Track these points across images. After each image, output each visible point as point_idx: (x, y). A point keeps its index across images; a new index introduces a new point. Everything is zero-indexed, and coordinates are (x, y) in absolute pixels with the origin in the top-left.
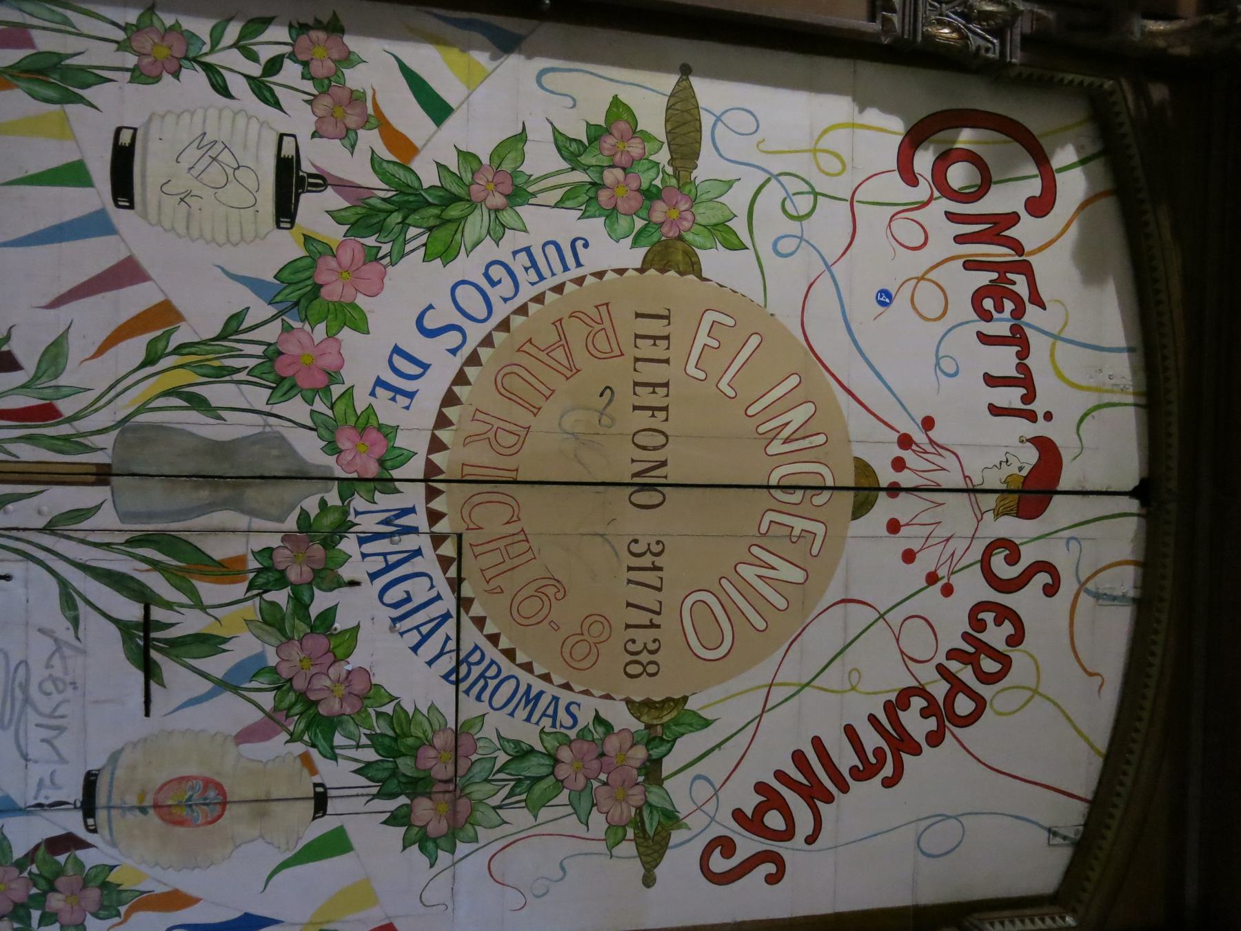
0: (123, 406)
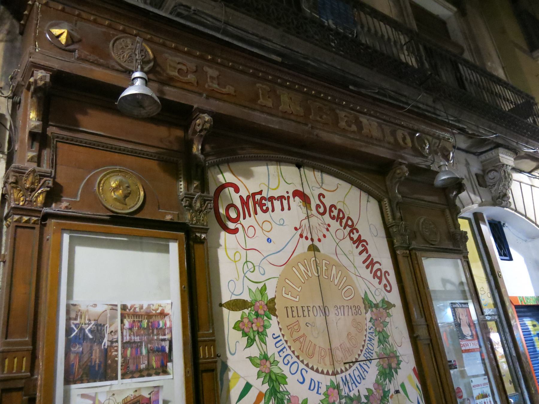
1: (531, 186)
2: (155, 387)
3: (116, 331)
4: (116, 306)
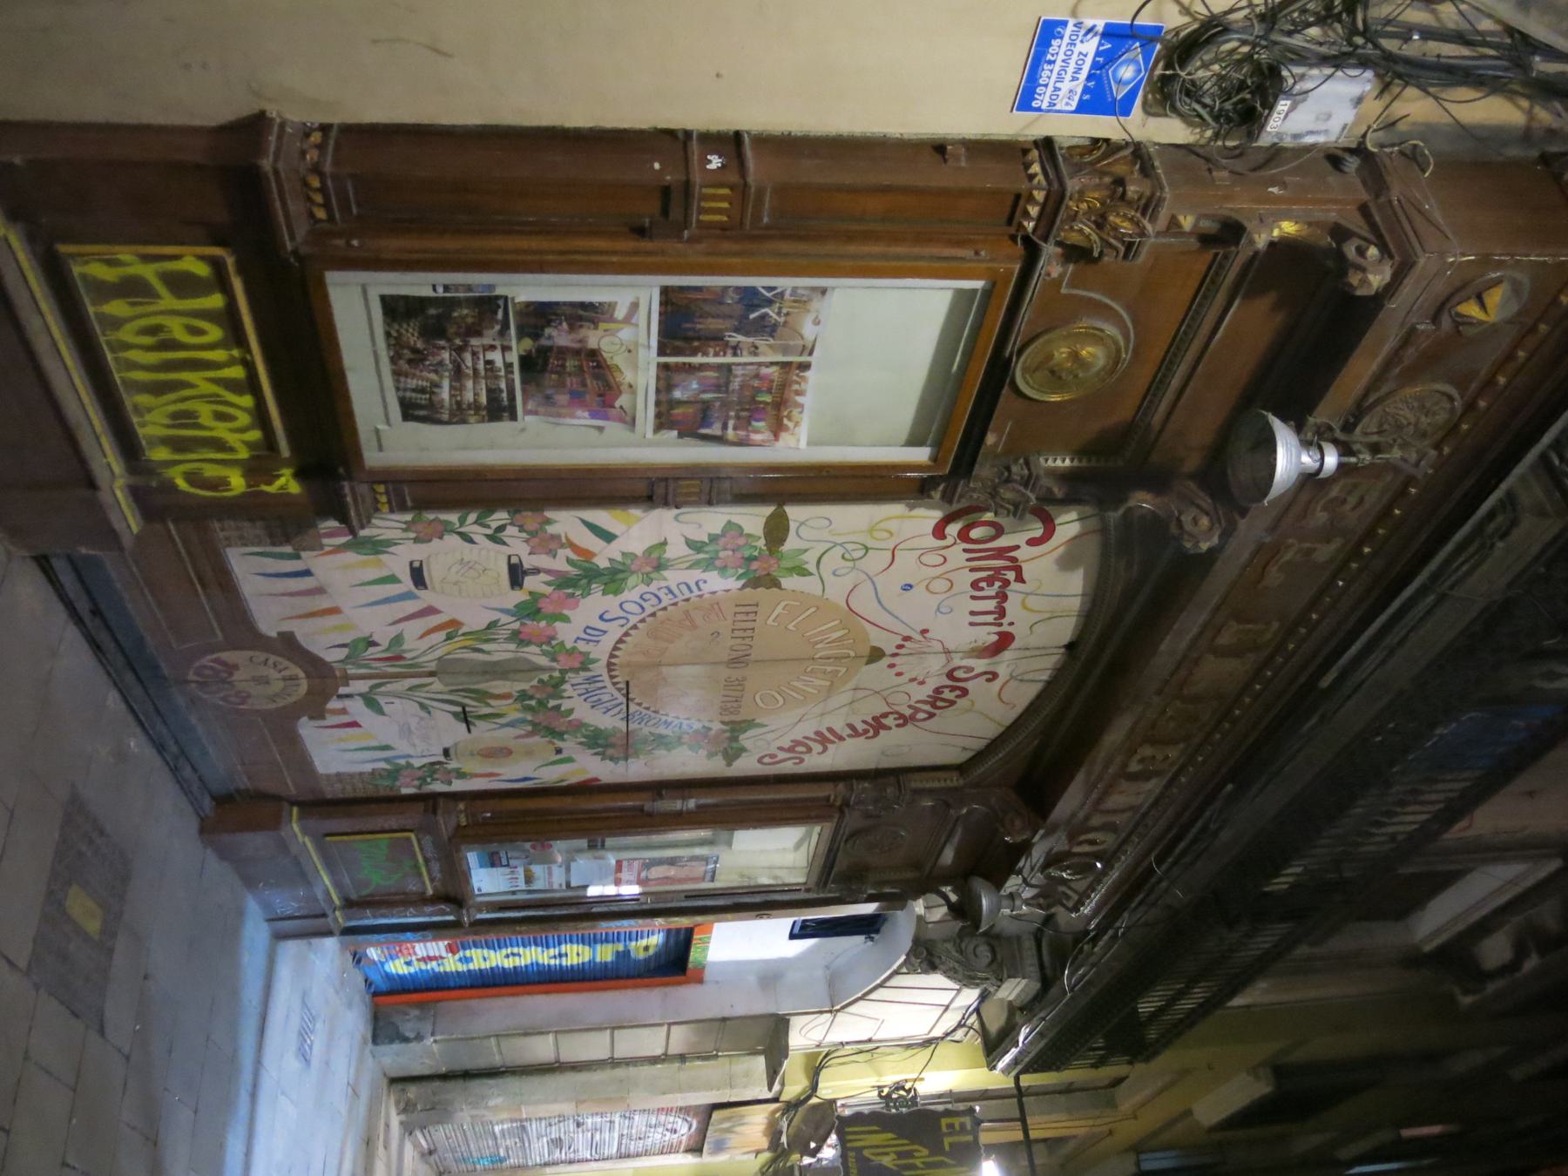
0: (438, 653)
1: (947, 1007)
2: (634, 420)
3: (756, 354)
4: (811, 354)
